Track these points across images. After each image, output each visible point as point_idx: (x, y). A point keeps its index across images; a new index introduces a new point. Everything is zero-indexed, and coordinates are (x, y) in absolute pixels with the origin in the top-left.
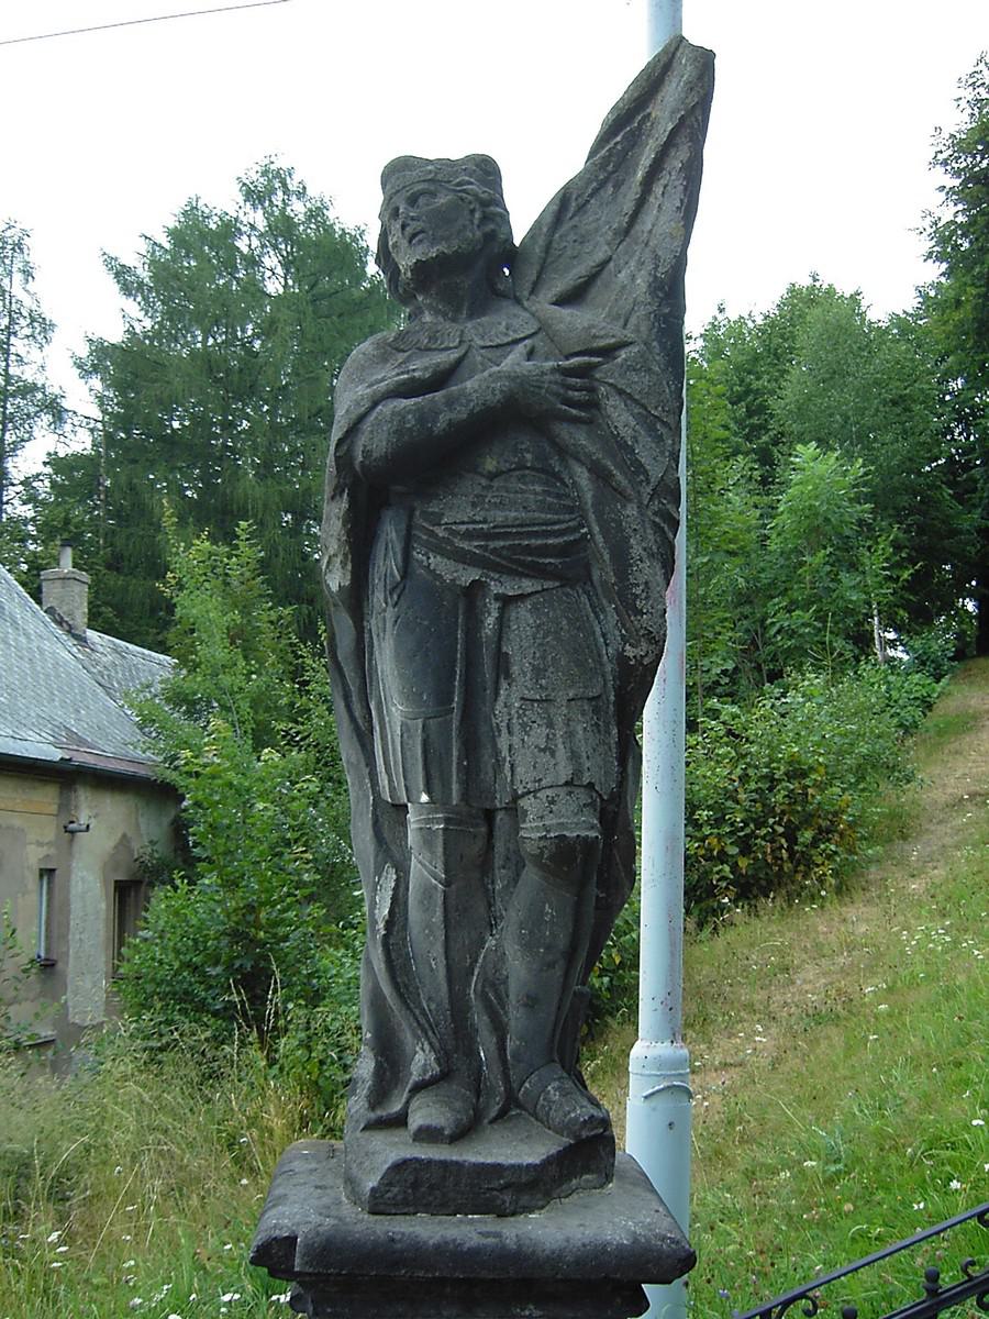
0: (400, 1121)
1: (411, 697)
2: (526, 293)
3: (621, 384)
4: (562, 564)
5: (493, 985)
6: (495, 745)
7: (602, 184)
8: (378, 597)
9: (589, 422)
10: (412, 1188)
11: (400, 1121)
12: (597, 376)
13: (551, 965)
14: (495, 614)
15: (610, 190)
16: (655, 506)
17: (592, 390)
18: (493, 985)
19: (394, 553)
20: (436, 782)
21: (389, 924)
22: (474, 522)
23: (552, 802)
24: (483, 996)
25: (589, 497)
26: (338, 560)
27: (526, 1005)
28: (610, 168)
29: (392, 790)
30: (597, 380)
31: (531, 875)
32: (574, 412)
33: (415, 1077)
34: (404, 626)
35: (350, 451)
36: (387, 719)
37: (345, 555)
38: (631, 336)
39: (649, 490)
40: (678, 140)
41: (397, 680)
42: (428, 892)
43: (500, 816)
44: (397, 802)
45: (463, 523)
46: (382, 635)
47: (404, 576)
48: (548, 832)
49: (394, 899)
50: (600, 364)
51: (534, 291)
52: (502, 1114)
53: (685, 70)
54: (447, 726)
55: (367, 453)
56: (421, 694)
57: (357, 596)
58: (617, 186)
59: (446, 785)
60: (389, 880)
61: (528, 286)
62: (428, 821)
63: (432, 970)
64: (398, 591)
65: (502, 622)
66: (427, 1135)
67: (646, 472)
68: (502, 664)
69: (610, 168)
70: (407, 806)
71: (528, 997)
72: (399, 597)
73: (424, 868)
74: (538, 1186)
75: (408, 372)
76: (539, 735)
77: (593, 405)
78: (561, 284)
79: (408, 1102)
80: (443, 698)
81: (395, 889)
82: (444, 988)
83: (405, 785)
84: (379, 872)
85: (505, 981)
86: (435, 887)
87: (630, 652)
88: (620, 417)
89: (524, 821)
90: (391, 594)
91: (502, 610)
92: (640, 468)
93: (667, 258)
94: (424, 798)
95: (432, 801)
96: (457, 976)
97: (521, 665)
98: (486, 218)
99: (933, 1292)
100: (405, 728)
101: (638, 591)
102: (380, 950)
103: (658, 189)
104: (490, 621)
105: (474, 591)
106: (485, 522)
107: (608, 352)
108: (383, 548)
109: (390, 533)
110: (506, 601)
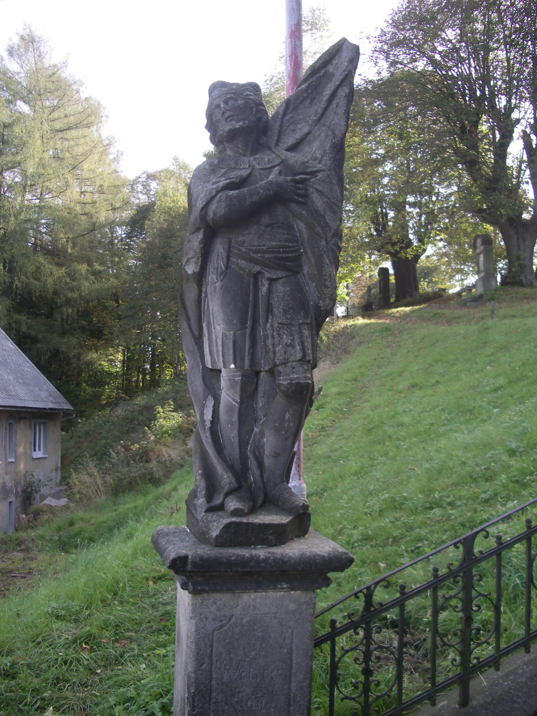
0: (221, 508)
1: (228, 322)
2: (273, 145)
3: (320, 188)
4: (288, 263)
5: (258, 448)
6: (265, 343)
7: (305, 98)
8: (212, 277)
9: (304, 204)
10: (234, 535)
11: (221, 508)
12: (309, 184)
13: (287, 439)
14: (267, 286)
15: (309, 101)
16: (333, 241)
17: (306, 190)
18: (258, 448)
19: (222, 258)
20: (238, 359)
21: (212, 422)
22: (259, 246)
23: (293, 368)
24: (254, 453)
25: (305, 236)
26: (194, 260)
27: (274, 457)
28: (309, 92)
29: (213, 362)
30: (309, 186)
31: (280, 399)
32: (300, 199)
33: (225, 490)
34: (225, 289)
35: (206, 213)
36: (213, 331)
37: (198, 258)
38: (324, 168)
39: (331, 234)
40: (344, 84)
41: (222, 314)
42: (230, 408)
43: (262, 374)
44: (214, 368)
45: (254, 246)
46: (213, 294)
47: (227, 267)
48: (292, 381)
49: (214, 411)
50: (310, 179)
51: (277, 144)
52: (264, 503)
53: (345, 56)
54: (244, 335)
55: (215, 214)
56: (233, 321)
57: (200, 277)
58: (312, 100)
59: (243, 360)
60: (210, 403)
61: (274, 142)
62: (234, 376)
63: (231, 442)
64: (224, 274)
65: (270, 291)
66: (236, 513)
67: (329, 227)
68: (269, 310)
69: (309, 92)
70: (220, 371)
71: (275, 453)
72: (224, 277)
73: (228, 396)
74: (279, 535)
75: (230, 179)
76: (286, 339)
77: (306, 196)
78: (290, 141)
79: (224, 500)
80: (243, 323)
81: (214, 407)
82: (237, 450)
83: (223, 361)
84: (205, 399)
85: (263, 447)
86: (235, 406)
87: (321, 303)
88: (318, 202)
89: (279, 376)
90: (220, 276)
91: (270, 285)
92: (327, 225)
93: (338, 134)
94: (232, 366)
95: (236, 367)
96: (243, 443)
97: (278, 308)
98: (257, 111)
99: (436, 576)
100: (224, 336)
101: (326, 278)
102: (208, 434)
103: (334, 105)
104: (264, 289)
105: (256, 276)
106: (264, 246)
107: (313, 174)
108: (216, 257)
109: (219, 248)
110: (271, 281)
